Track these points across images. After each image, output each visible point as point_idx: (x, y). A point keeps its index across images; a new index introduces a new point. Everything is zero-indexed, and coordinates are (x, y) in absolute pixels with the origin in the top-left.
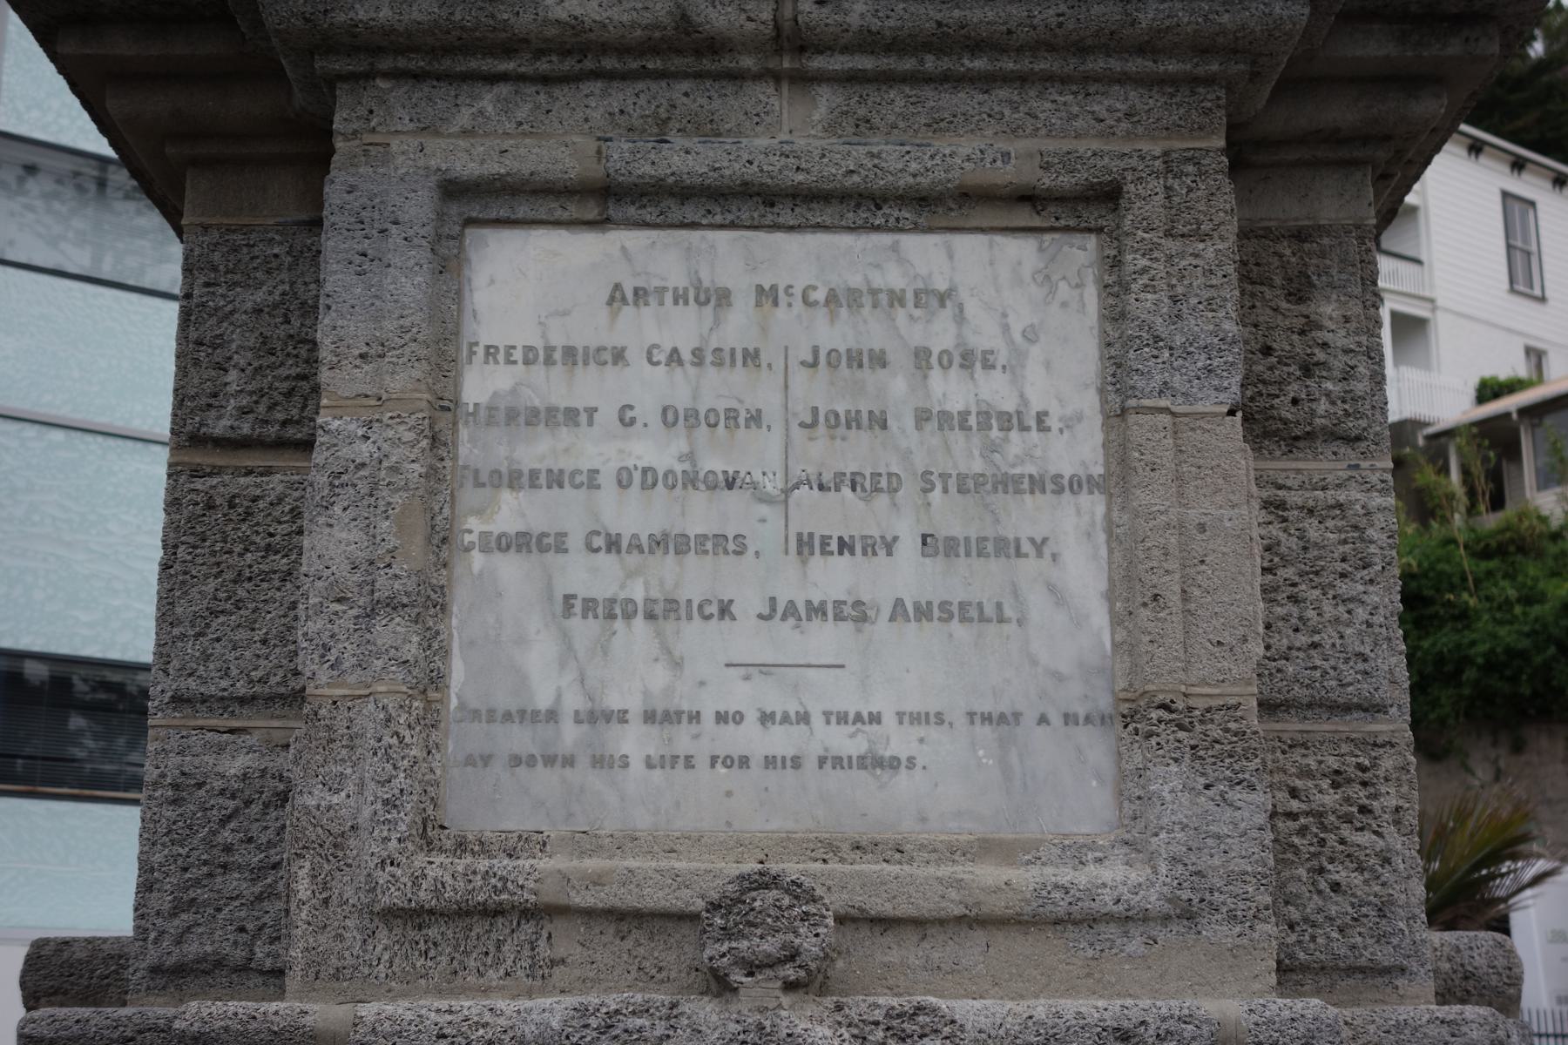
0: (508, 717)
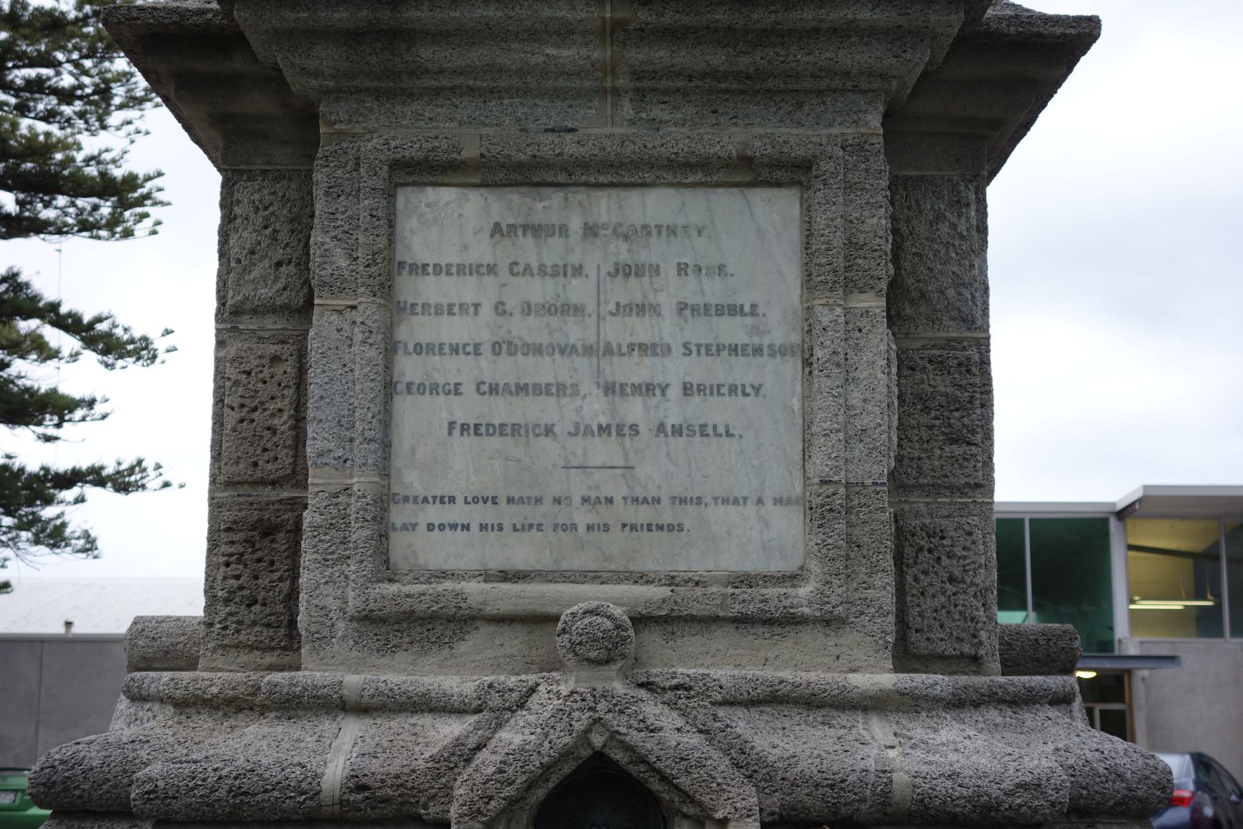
0: (425, 500)
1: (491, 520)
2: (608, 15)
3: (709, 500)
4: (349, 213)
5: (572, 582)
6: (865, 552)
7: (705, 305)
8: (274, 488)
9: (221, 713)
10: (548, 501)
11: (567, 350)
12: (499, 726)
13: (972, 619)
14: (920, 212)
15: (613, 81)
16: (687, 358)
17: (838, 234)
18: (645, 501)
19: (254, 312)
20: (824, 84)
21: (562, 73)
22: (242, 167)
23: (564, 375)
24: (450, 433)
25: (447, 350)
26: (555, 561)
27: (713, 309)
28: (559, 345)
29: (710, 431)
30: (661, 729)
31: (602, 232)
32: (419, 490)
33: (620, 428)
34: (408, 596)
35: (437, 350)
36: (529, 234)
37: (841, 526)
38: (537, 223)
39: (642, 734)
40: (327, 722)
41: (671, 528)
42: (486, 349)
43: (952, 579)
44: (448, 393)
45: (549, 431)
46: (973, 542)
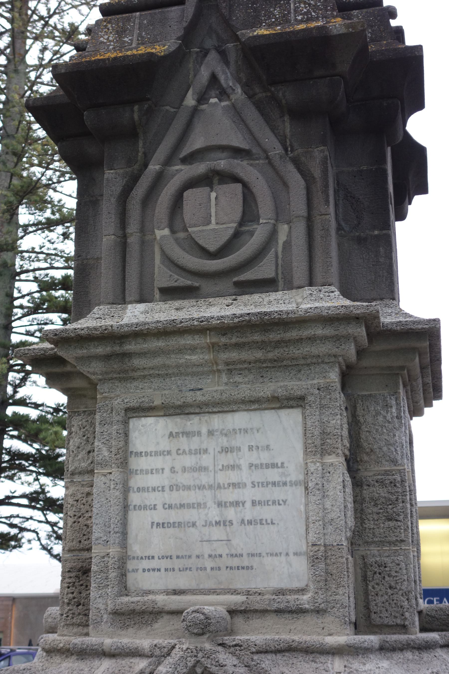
0: (142, 558)
1: (169, 567)
2: (208, 341)
3: (264, 554)
4: (109, 432)
5: (205, 594)
6: (334, 578)
7: (261, 464)
8: (88, 552)
9: (65, 656)
10: (194, 557)
11: (201, 487)
12: (159, 664)
13: (401, 607)
14: (369, 411)
15: (216, 367)
16: (253, 489)
17: (317, 429)
18: (236, 556)
19: (80, 473)
20: (309, 361)
21: (195, 365)
22: (75, 410)
23: (200, 499)
24: (152, 527)
25: (150, 489)
26: (197, 584)
27: (264, 466)
28: (198, 485)
29: (264, 522)
30: (225, 665)
31: (216, 433)
32: (139, 553)
33: (224, 522)
34: (132, 603)
35: (146, 490)
36: (185, 436)
37: (322, 566)
38: (188, 431)
39: (217, 668)
40: (97, 661)
41: (248, 568)
42: (167, 489)
43: (391, 587)
44: (151, 509)
45: (194, 524)
46: (400, 569)
